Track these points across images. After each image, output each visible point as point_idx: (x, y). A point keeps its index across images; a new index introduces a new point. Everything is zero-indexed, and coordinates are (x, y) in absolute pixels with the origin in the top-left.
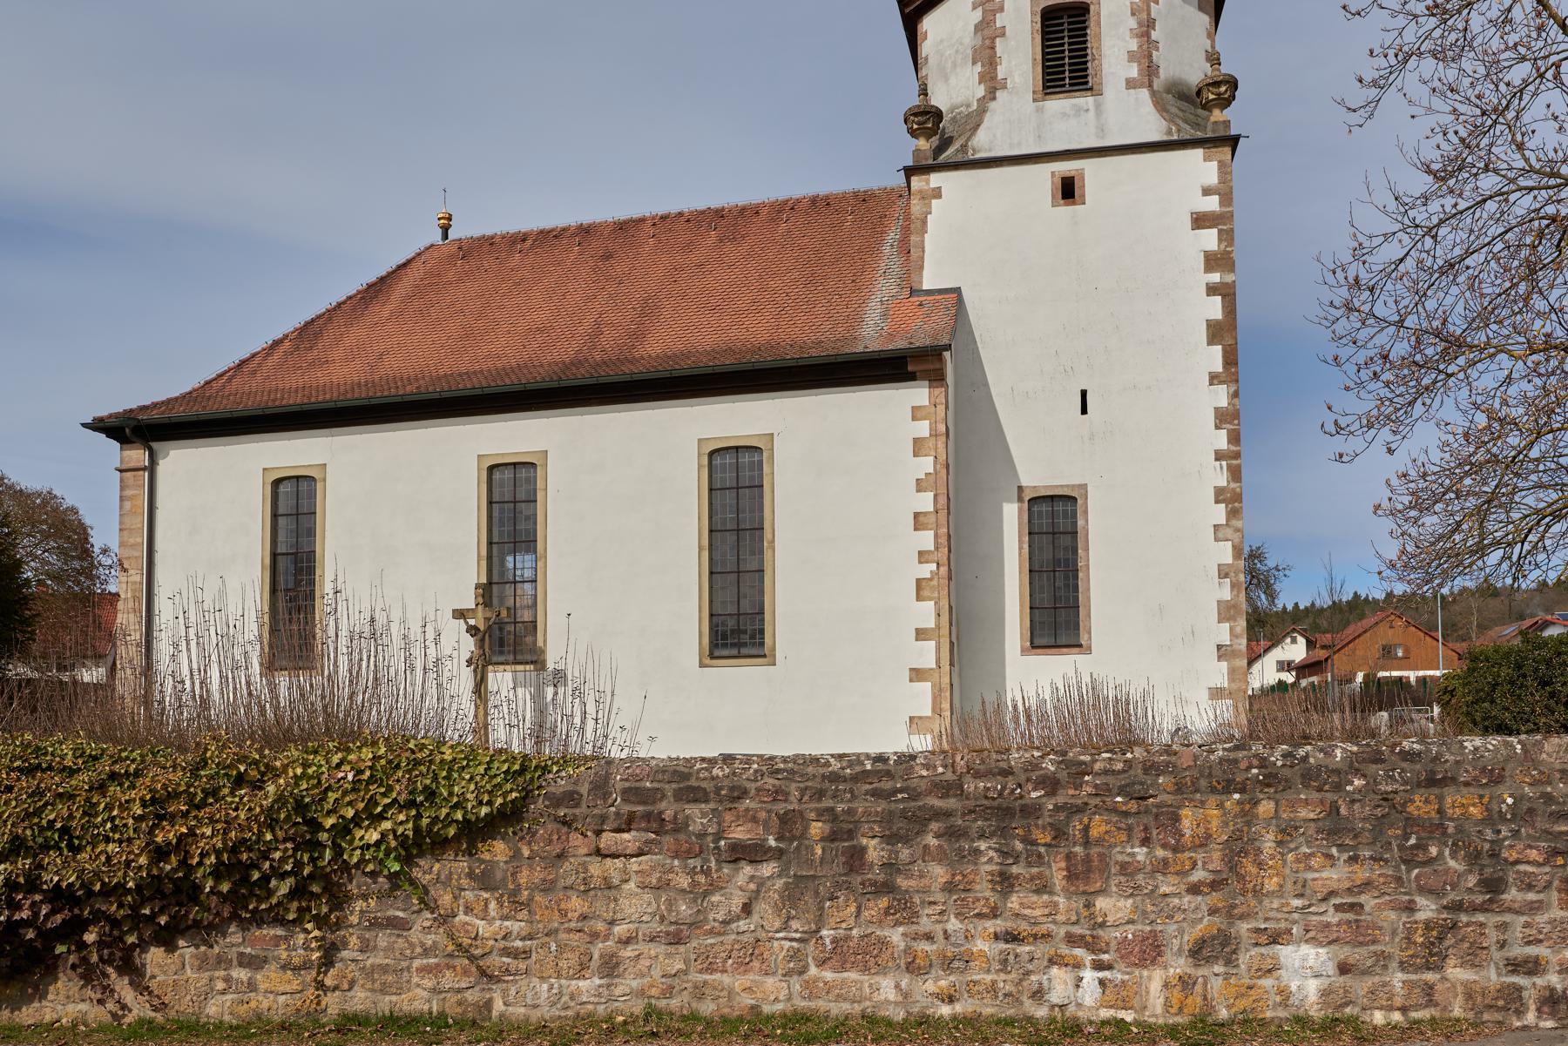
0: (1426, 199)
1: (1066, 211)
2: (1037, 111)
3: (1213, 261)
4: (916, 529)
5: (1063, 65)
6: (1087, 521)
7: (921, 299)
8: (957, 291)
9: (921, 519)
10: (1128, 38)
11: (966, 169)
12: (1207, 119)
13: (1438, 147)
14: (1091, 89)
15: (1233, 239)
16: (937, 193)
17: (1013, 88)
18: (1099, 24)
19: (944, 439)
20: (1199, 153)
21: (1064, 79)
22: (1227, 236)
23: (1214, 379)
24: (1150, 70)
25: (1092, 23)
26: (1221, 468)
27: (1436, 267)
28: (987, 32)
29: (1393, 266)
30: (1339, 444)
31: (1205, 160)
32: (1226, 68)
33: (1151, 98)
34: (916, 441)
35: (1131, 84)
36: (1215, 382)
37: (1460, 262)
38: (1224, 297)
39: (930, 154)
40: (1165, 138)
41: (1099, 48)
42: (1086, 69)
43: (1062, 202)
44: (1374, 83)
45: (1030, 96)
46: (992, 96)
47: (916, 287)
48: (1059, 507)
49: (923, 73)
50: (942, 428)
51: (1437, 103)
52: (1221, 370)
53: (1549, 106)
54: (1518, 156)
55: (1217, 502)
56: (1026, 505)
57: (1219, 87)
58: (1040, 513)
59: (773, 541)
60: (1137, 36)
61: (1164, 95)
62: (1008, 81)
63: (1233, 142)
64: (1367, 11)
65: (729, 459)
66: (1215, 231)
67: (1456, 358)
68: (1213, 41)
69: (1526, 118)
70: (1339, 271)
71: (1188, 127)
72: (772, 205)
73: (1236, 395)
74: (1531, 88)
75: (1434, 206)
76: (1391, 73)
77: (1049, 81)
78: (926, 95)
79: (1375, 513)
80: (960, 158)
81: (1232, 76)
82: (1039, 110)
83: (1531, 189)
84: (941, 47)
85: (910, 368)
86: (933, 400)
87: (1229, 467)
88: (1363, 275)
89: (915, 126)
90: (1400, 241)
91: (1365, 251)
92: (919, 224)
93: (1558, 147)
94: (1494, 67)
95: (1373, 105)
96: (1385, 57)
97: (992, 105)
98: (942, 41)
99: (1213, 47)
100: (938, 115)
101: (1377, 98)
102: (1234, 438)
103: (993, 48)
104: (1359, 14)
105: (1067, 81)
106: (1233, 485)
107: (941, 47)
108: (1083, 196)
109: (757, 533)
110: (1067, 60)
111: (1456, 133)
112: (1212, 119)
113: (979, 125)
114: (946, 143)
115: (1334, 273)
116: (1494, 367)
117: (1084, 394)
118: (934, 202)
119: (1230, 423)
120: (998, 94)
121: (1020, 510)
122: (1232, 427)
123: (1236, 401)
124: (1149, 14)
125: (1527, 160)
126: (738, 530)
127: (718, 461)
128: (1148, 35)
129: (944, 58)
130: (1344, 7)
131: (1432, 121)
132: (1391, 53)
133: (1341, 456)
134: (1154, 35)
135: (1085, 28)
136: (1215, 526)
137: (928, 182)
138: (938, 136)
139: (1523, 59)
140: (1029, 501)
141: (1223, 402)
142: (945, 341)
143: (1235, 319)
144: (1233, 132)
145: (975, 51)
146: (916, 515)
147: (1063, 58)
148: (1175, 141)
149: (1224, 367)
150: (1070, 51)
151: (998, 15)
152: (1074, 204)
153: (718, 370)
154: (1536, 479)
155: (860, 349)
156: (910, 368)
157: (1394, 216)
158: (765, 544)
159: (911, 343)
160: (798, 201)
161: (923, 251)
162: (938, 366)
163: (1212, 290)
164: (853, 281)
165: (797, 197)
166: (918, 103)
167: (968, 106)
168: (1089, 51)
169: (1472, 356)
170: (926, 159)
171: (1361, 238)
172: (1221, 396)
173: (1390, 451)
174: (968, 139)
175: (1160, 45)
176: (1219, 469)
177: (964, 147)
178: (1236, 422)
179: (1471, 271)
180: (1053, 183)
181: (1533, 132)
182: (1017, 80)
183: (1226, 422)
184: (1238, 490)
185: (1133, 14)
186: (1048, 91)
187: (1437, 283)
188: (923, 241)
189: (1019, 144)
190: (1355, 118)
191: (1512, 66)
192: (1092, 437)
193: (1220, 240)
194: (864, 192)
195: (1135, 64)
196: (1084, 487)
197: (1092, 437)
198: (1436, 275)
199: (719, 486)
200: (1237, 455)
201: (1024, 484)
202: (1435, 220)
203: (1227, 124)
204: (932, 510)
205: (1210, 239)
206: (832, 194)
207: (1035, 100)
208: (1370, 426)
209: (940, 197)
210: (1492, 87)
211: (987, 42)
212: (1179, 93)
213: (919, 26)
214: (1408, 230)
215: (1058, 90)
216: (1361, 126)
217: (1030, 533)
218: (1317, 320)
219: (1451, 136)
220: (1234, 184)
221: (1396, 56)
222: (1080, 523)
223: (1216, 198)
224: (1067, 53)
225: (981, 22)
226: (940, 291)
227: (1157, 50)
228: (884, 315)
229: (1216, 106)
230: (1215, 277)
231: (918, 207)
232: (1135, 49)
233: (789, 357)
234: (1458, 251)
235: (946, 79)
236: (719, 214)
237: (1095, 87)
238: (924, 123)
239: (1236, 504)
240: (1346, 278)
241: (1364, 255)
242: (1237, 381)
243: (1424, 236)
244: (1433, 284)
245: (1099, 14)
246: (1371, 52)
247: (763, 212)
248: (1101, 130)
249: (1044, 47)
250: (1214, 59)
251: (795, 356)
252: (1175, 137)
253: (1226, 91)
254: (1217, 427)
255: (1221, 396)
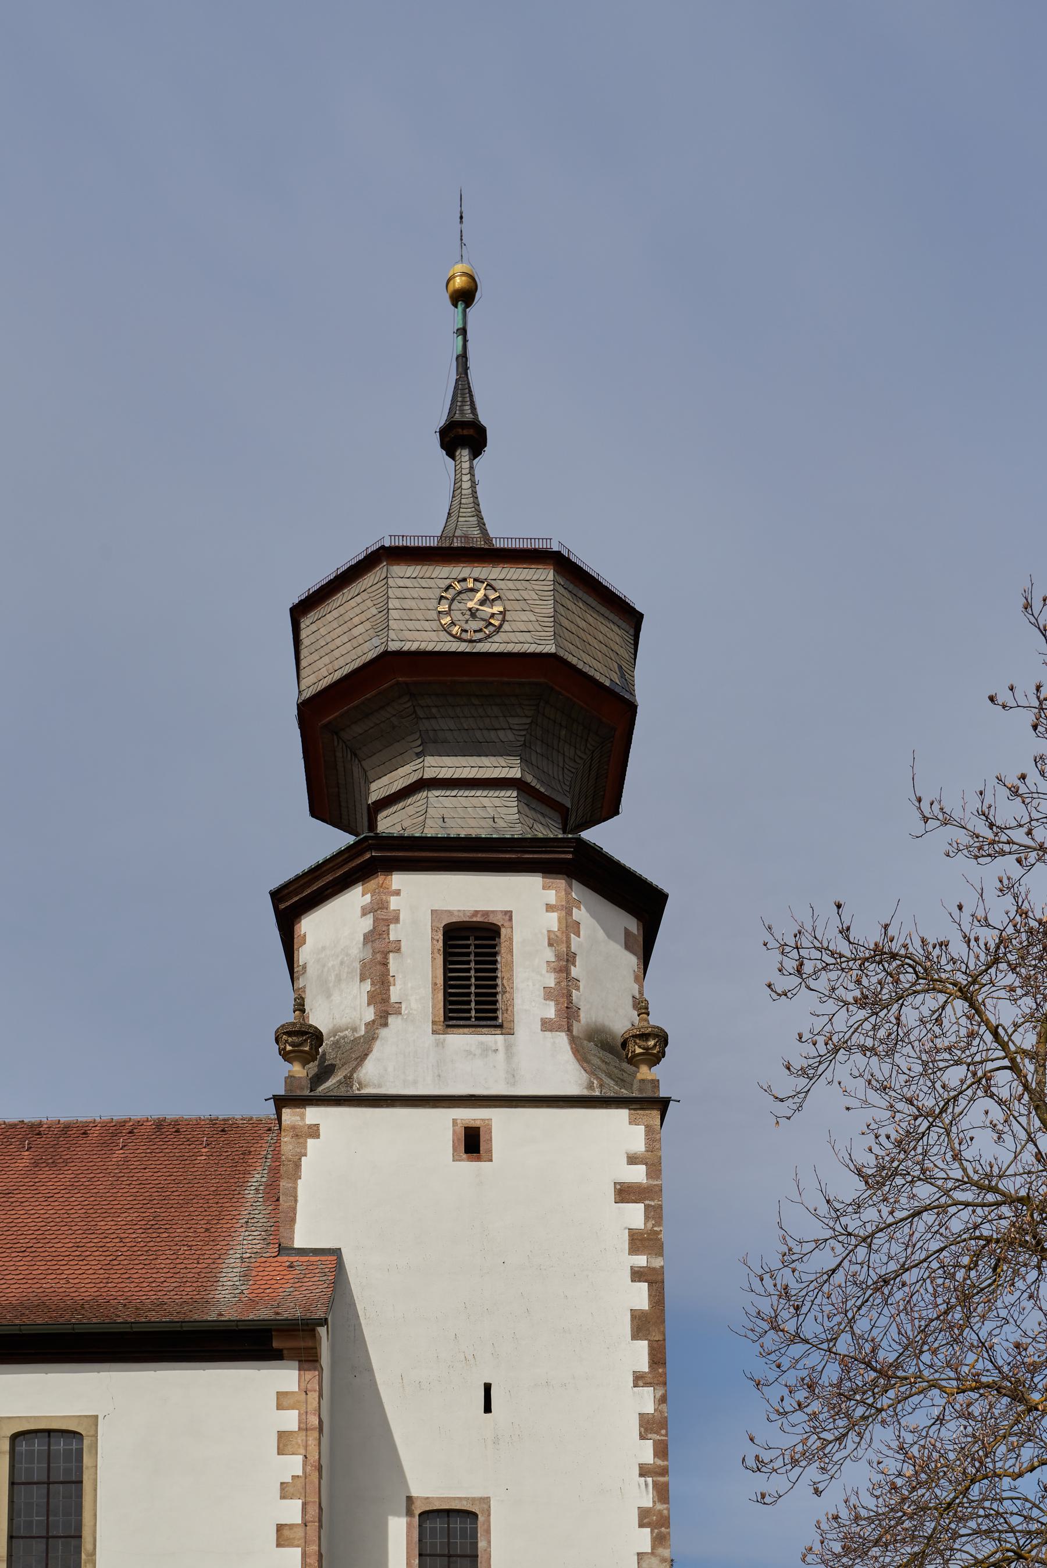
0: (858, 1206)
1: (469, 1167)
2: (437, 1045)
3: (638, 1241)
4: (278, 1545)
5: (469, 994)
6: (489, 1542)
7: (292, 1259)
8: (337, 1252)
9: (286, 1532)
10: (544, 971)
11: (350, 1106)
12: (633, 1075)
13: (871, 1150)
14: (501, 1026)
15: (661, 1218)
16: (314, 1132)
17: (409, 1014)
18: (511, 951)
19: (316, 1434)
20: (623, 1114)
21: (469, 1011)
22: (654, 1213)
23: (639, 1379)
24: (569, 1013)
25: (503, 949)
26: (646, 1485)
27: (870, 1282)
28: (378, 945)
29: (825, 1277)
30: (760, 1482)
31: (630, 1123)
32: (655, 1020)
33: (570, 1044)
34: (281, 1435)
35: (547, 1025)
36: (640, 1383)
37: (895, 1279)
38: (651, 1283)
39: (306, 1083)
40: (585, 1092)
41: (511, 979)
42: (495, 1002)
43: (465, 1156)
44: (803, 1072)
45: (429, 1027)
46: (383, 1021)
47: (285, 1243)
48: (457, 1524)
49: (300, 983)
50: (314, 1421)
51: (874, 1097)
52: (647, 1370)
53: (987, 1113)
54: (956, 1165)
55: (641, 1525)
56: (416, 1520)
57: (647, 1040)
58: (433, 1530)
59: (94, 1553)
60: (555, 970)
61: (585, 1042)
62: (403, 1006)
63: (662, 1105)
64: (794, 992)
65: (38, 1445)
66: (641, 1207)
67: (886, 1392)
68: (641, 987)
69: (964, 1123)
70: (766, 1277)
71: (612, 1083)
72: (105, 1125)
73: (663, 1400)
74: (969, 1092)
75: (870, 1214)
76: (820, 1063)
77: (452, 1011)
78: (303, 1011)
79: (804, 1560)
80: (342, 1092)
81: (662, 1030)
82: (440, 1045)
83: (967, 1205)
84: (323, 955)
85: (276, 1344)
86: (303, 1385)
87: (655, 1484)
88: (793, 1285)
89: (289, 1048)
90: (833, 1249)
91: (795, 1257)
92: (291, 1166)
93: (993, 1161)
94: (930, 1070)
95: (802, 1095)
96: (814, 1044)
97: (383, 1032)
98: (324, 948)
99: (641, 993)
100: (317, 1037)
101: (806, 1089)
102: (661, 1450)
103: (385, 964)
104: (786, 995)
105: (473, 1013)
106: (659, 1507)
107: (323, 955)
108: (490, 1151)
109: (73, 1542)
110: (473, 989)
111: (888, 1137)
112: (639, 1076)
113: (367, 1055)
114: (326, 1072)
115: (762, 1280)
116: (927, 1402)
117: (488, 1388)
118: (311, 1142)
119: (657, 1433)
120: (391, 1019)
121: (409, 1526)
122: (658, 1437)
123: (663, 1407)
124: (569, 947)
125: (965, 1170)
126: (48, 1538)
127: (23, 1447)
128: (568, 972)
129: (326, 969)
130: (769, 986)
131: (868, 1115)
132: (821, 1040)
133: (763, 1496)
134: (574, 972)
135: (495, 954)
136: (638, 1554)
137: (303, 1117)
138: (316, 1063)
139: (958, 1063)
140: (420, 1515)
141: (649, 1408)
142: (320, 1314)
143: (663, 1311)
144: (663, 1093)
145: (364, 966)
146: (280, 1528)
147: (469, 987)
148: (597, 1097)
149: (650, 1367)
150: (477, 979)
151: (392, 926)
152: (479, 1159)
153: (25, 1330)
154: (974, 1526)
155: (213, 1317)
156: (276, 1344)
157: (826, 1221)
158: (83, 1556)
159: (278, 1314)
160: (139, 1123)
161: (296, 1201)
162: (310, 1344)
163: (637, 1275)
164: (207, 1230)
165: (138, 1118)
166: (293, 1020)
167: (355, 1030)
168: (499, 982)
169: (903, 1389)
170: (302, 1089)
171: (791, 1243)
172: (646, 1401)
173: (818, 1492)
174: (354, 1070)
175: (581, 984)
176: (643, 1486)
177: (348, 1080)
178: (663, 1432)
179: (906, 1289)
180: (454, 1132)
181: (972, 1139)
182: (414, 1005)
183: (652, 1431)
184: (665, 1512)
185: (550, 945)
186: (451, 1023)
187: (871, 1299)
188: (295, 1189)
189: (415, 1082)
190: (783, 1109)
191: (947, 1067)
192: (496, 1441)
193: (647, 1218)
194: (224, 1120)
195: (552, 1003)
196: (486, 1500)
197: (496, 1441)
198: (869, 1292)
199: (23, 1480)
200: (664, 1471)
201: (415, 1493)
202: (870, 1229)
203: (655, 1084)
204: (300, 1522)
205: (635, 1215)
206: (182, 1119)
207: (434, 1032)
208: (795, 1462)
209: (318, 1136)
210: (929, 1084)
211: (379, 957)
212: (602, 1042)
213: (296, 927)
214: (840, 1238)
215: (462, 1023)
216: (789, 1118)
217: (420, 1555)
218: (743, 1331)
219: (883, 1139)
220: (663, 1153)
221: (826, 1044)
222: (482, 1544)
223: (642, 1168)
224: (473, 980)
225: (371, 932)
226: (316, 1252)
227: (578, 989)
228: (245, 1276)
229: (644, 1062)
230: (641, 1261)
231: (290, 1147)
232: (553, 985)
233: (120, 1320)
234: (893, 1266)
235: (329, 996)
236: (35, 1130)
237: (505, 1025)
238: (300, 1044)
239: (663, 1529)
240: (775, 1285)
241: (794, 1261)
242: (665, 1384)
243: (856, 1246)
244: (867, 1301)
245: (511, 939)
246: (800, 1036)
247: (94, 1133)
248: (512, 1076)
249: (446, 970)
250: (642, 1007)
251: (129, 1320)
252: (597, 1093)
253: (655, 1045)
254: (642, 1437)
255: (646, 1401)
